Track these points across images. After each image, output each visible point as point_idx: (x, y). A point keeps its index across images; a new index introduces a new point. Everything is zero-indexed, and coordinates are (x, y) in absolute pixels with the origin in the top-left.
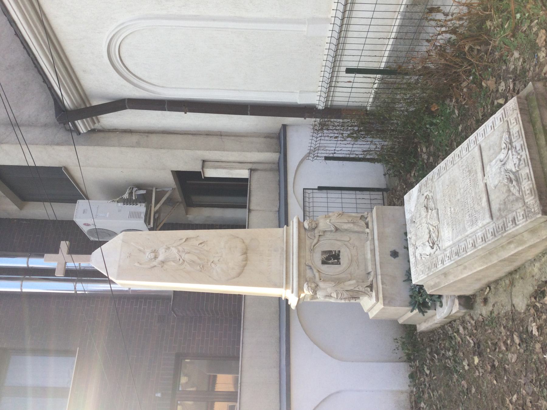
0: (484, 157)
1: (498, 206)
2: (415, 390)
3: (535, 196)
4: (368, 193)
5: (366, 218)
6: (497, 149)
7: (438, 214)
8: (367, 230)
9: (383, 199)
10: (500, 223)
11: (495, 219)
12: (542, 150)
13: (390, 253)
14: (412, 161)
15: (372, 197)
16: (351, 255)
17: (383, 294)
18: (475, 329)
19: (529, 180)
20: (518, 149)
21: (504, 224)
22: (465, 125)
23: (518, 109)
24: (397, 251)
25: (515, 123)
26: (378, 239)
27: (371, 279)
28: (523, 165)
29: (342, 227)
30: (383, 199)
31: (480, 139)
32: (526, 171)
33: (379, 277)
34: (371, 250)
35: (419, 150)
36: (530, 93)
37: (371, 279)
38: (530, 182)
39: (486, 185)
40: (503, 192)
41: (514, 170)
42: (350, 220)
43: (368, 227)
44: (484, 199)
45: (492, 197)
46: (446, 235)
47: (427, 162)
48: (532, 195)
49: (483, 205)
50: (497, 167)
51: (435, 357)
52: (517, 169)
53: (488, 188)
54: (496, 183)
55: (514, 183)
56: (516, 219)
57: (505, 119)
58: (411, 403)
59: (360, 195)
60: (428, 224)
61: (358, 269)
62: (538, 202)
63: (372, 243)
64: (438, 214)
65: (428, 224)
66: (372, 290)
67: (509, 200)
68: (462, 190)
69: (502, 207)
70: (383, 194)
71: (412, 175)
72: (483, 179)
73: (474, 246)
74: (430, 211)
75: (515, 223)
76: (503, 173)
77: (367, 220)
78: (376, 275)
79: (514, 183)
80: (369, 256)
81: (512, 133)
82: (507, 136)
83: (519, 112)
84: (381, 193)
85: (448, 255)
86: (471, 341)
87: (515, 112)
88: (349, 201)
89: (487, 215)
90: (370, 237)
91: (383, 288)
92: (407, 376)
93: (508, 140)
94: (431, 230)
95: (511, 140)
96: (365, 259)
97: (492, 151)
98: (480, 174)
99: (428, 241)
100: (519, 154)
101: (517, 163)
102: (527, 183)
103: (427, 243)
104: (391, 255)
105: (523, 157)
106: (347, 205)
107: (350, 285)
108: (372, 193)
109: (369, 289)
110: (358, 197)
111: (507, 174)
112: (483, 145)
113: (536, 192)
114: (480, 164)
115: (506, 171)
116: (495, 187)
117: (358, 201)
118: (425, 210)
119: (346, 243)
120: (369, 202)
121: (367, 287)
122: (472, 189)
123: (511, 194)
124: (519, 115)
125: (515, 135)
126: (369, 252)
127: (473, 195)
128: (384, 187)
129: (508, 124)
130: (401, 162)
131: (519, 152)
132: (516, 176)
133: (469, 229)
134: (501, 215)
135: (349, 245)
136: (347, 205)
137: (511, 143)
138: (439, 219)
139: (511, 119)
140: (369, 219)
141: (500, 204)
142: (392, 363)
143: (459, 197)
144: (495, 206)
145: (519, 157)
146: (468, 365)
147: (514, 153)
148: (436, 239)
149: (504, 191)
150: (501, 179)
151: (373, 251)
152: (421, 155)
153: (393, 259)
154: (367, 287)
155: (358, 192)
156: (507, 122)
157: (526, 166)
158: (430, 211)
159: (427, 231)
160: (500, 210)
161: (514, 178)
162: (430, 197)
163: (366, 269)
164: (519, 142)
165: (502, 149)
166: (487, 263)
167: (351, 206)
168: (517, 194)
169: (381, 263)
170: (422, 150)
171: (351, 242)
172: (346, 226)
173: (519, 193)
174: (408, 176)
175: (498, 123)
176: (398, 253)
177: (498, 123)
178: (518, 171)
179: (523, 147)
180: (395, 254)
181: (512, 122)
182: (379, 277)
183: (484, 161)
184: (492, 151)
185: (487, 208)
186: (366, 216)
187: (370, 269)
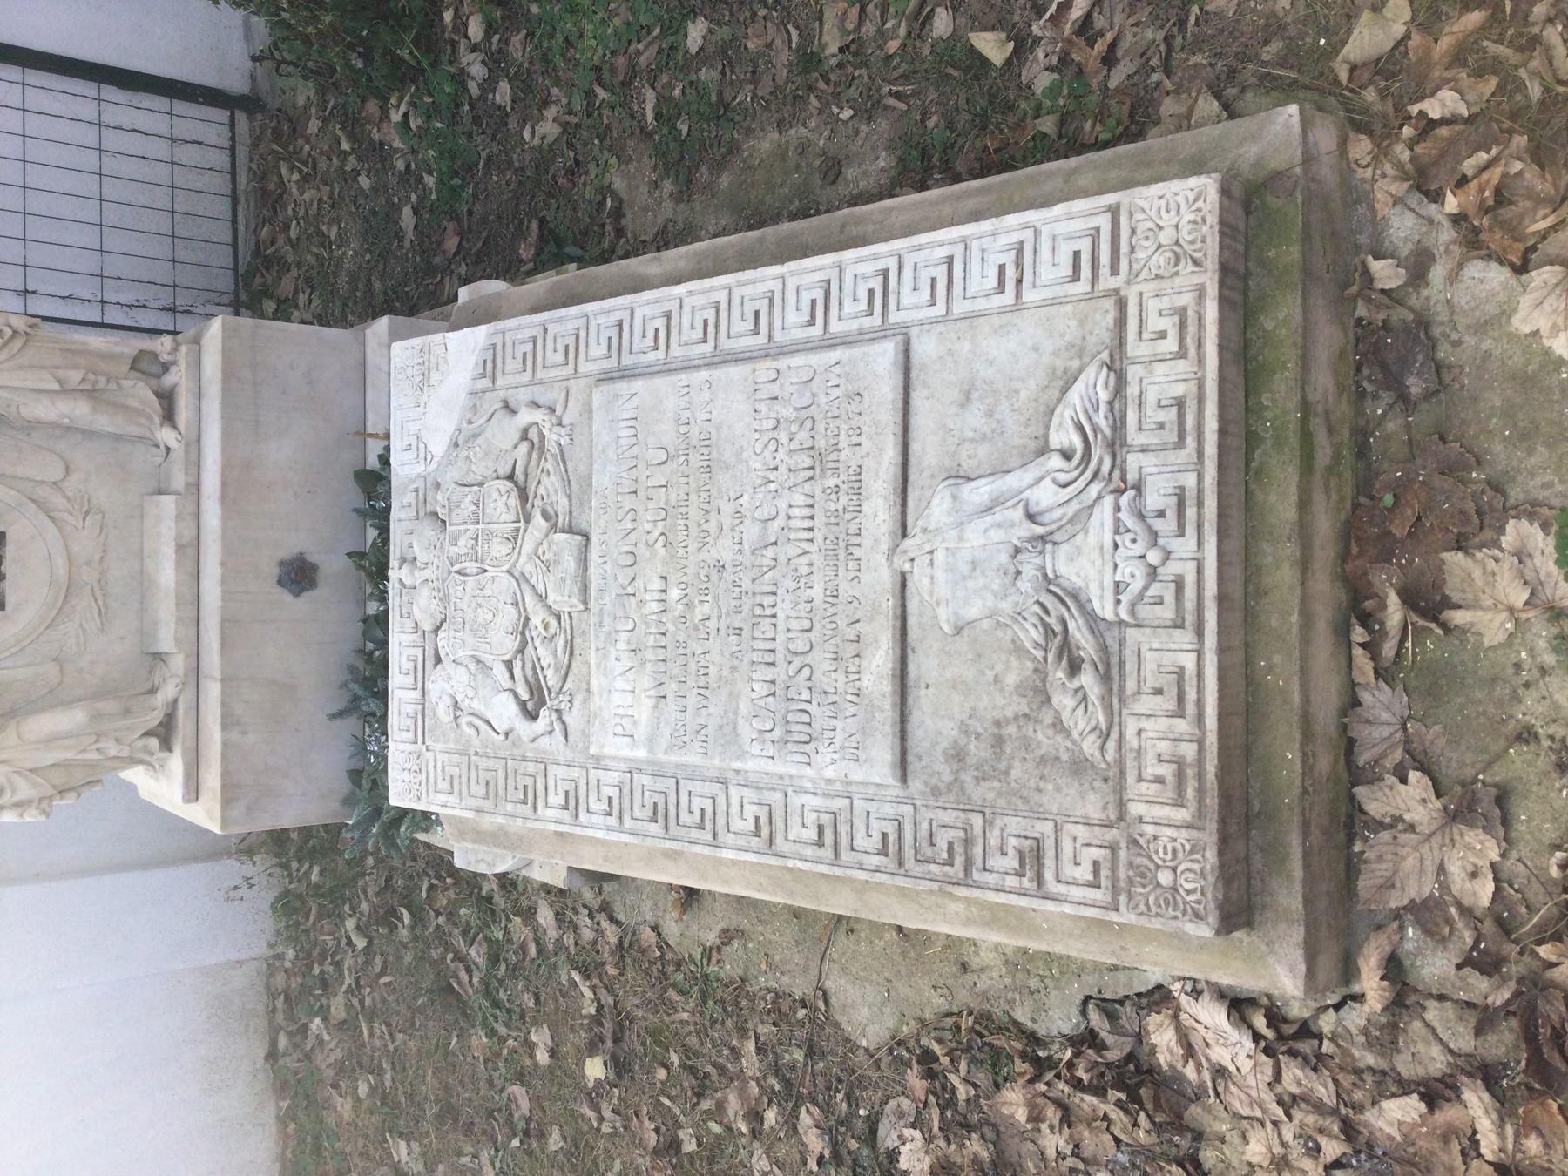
0: (920, 422)
1: (950, 731)
2: (291, 954)
3: (1200, 813)
4: (161, 103)
5: (166, 367)
6: (1017, 432)
7: (584, 562)
8: (167, 436)
9: (233, 149)
10: (947, 823)
11: (916, 785)
12: (1267, 548)
13: (276, 571)
14: (404, 53)
15: (184, 129)
16: (70, 560)
17: (225, 774)
18: (616, 966)
19: (1180, 713)
20: (1153, 501)
21: (968, 842)
22: (724, 33)
23: (1212, 264)
24: (312, 558)
25: (1170, 344)
26: (224, 498)
27: (168, 692)
28: (1167, 612)
29: (24, 412)
30: (233, 149)
31: (911, 304)
32: (1176, 655)
33: (213, 691)
34: (180, 548)
35: (448, 16)
36: (1277, 175)
37: (168, 692)
38: (1182, 726)
39: (904, 585)
40: (996, 679)
41: (1105, 610)
42: (75, 377)
43: (169, 416)
44: (880, 659)
45: (924, 665)
46: (617, 698)
47: (483, 98)
48: (1179, 803)
49: (867, 681)
50: (997, 535)
51: (400, 919)
52: (1124, 616)
53: (912, 606)
54: (973, 612)
55: (1087, 679)
56: (1049, 862)
57: (1107, 282)
58: (272, 995)
59: (122, 107)
60: (521, 579)
61: (102, 629)
62: (1211, 855)
63: (191, 508)
64: (584, 562)
65: (521, 579)
66: (166, 745)
67: (1027, 744)
68: (751, 532)
69: (978, 751)
70: (232, 125)
71: (396, 117)
72: (893, 550)
73: (765, 832)
74: (538, 521)
75: (1039, 879)
76: (1025, 585)
77: (168, 380)
78: (196, 672)
79: (1087, 679)
80: (167, 574)
81: (1132, 390)
82: (1104, 396)
83: (1212, 290)
84: (222, 115)
85: (607, 791)
86: (588, 994)
87: (1189, 277)
88: (63, 130)
89: (882, 753)
90: (179, 480)
91: (225, 744)
92: (266, 906)
93: (1102, 421)
94: (536, 621)
95: (1119, 425)
96: (143, 584)
97: (975, 419)
98: (878, 512)
99: (509, 665)
100: (1154, 535)
101: (1137, 585)
102: (1163, 724)
103: (500, 672)
104: (280, 583)
105: (1173, 568)
106: (52, 154)
107: (51, 740)
108: (180, 107)
109: (154, 743)
110: (112, 115)
111: (1049, 601)
112: (925, 348)
113: (1212, 801)
114: (891, 453)
115: (1048, 581)
116: (959, 630)
117: (112, 140)
118: (514, 500)
119: (43, 492)
120: (160, 149)
121: (147, 734)
122: (816, 558)
123: (1048, 718)
124: (1212, 311)
125: (1154, 415)
126: (168, 552)
127: (817, 593)
128: (236, 83)
129: (1121, 323)
130: (351, 46)
131: (1157, 524)
132: (1104, 648)
133: (756, 749)
134: (956, 783)
135: (58, 501)
136: (52, 154)
137: (1117, 443)
138: (585, 589)
139: (1152, 305)
140: (178, 377)
141: (965, 730)
142: (209, 865)
143: (723, 550)
144: (935, 723)
145: (1154, 557)
146: (553, 1053)
147: (1128, 519)
148: (551, 679)
149: (1011, 679)
150: (1006, 606)
151: (190, 552)
152: (454, 45)
153: (288, 597)
154: (147, 734)
155: (110, 92)
156: (1122, 305)
157: (1179, 625)
158: (538, 521)
159: (509, 616)
160: (958, 756)
161: (1078, 646)
162: (551, 447)
163: (146, 632)
164: (1176, 471)
165: (1043, 451)
166: (791, 894)
167: (68, 182)
168: (1090, 746)
169: (227, 622)
170: (461, 25)
171: (71, 485)
172: (44, 410)
173: (1102, 748)
174: (372, 107)
175: (1051, 270)
176: (314, 568)
177: (1051, 270)
178: (1121, 623)
179: (1191, 513)
180: (298, 575)
181: (1155, 323)
182: (213, 691)
183: (915, 448)
184: (975, 419)
185: (886, 714)
186: (165, 357)
187: (167, 639)
